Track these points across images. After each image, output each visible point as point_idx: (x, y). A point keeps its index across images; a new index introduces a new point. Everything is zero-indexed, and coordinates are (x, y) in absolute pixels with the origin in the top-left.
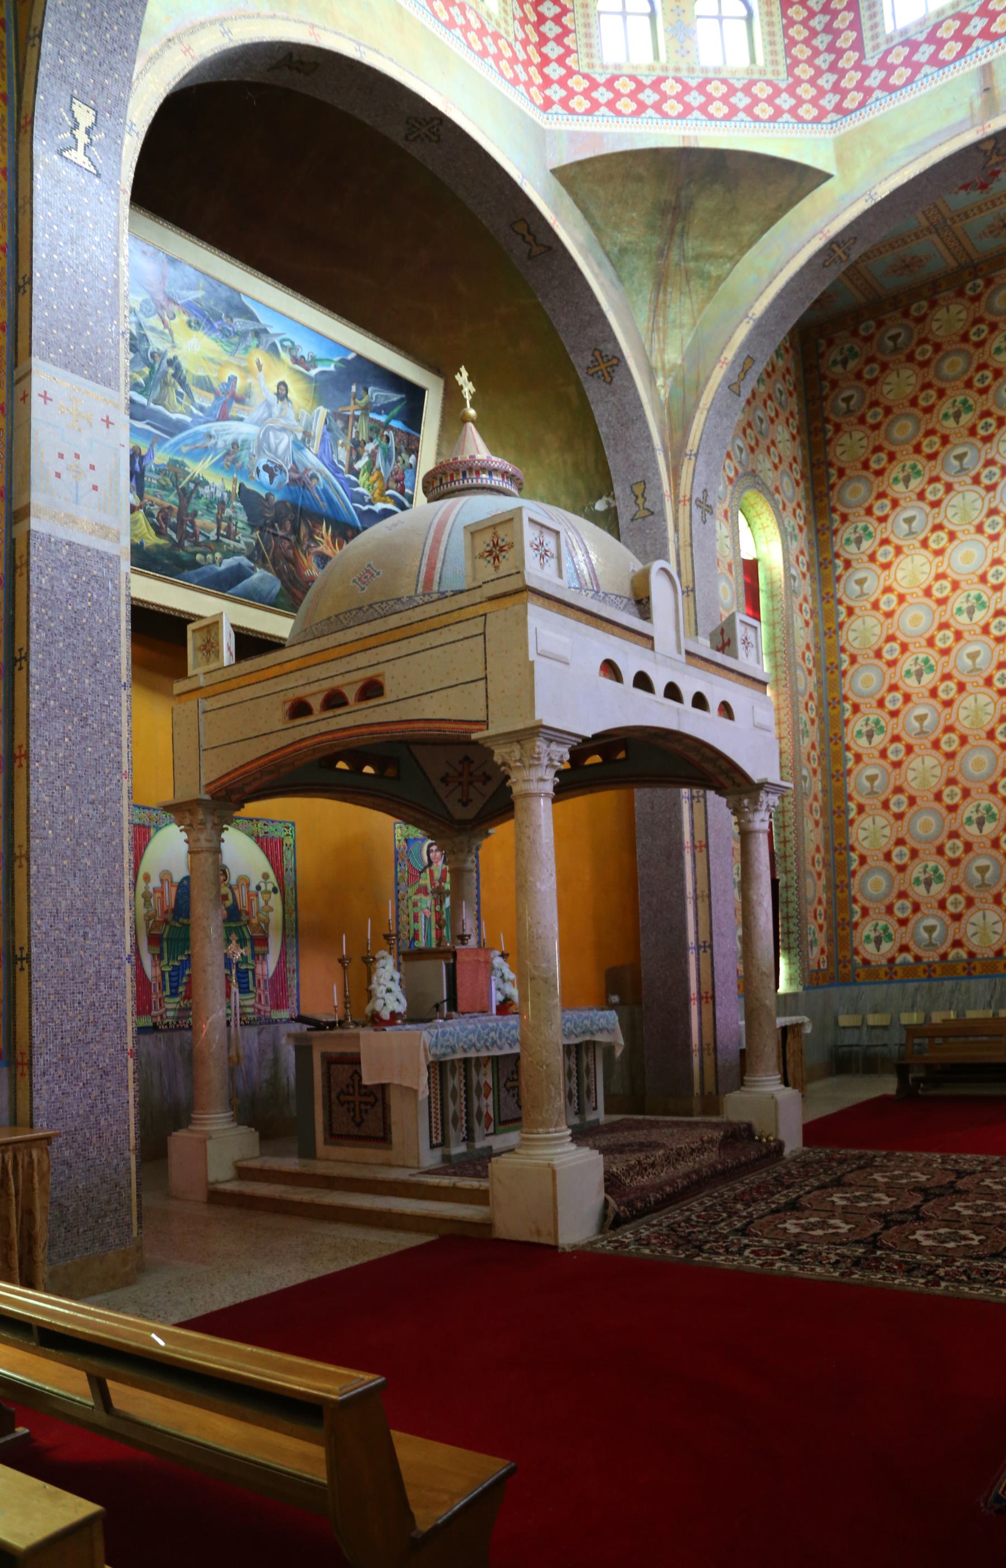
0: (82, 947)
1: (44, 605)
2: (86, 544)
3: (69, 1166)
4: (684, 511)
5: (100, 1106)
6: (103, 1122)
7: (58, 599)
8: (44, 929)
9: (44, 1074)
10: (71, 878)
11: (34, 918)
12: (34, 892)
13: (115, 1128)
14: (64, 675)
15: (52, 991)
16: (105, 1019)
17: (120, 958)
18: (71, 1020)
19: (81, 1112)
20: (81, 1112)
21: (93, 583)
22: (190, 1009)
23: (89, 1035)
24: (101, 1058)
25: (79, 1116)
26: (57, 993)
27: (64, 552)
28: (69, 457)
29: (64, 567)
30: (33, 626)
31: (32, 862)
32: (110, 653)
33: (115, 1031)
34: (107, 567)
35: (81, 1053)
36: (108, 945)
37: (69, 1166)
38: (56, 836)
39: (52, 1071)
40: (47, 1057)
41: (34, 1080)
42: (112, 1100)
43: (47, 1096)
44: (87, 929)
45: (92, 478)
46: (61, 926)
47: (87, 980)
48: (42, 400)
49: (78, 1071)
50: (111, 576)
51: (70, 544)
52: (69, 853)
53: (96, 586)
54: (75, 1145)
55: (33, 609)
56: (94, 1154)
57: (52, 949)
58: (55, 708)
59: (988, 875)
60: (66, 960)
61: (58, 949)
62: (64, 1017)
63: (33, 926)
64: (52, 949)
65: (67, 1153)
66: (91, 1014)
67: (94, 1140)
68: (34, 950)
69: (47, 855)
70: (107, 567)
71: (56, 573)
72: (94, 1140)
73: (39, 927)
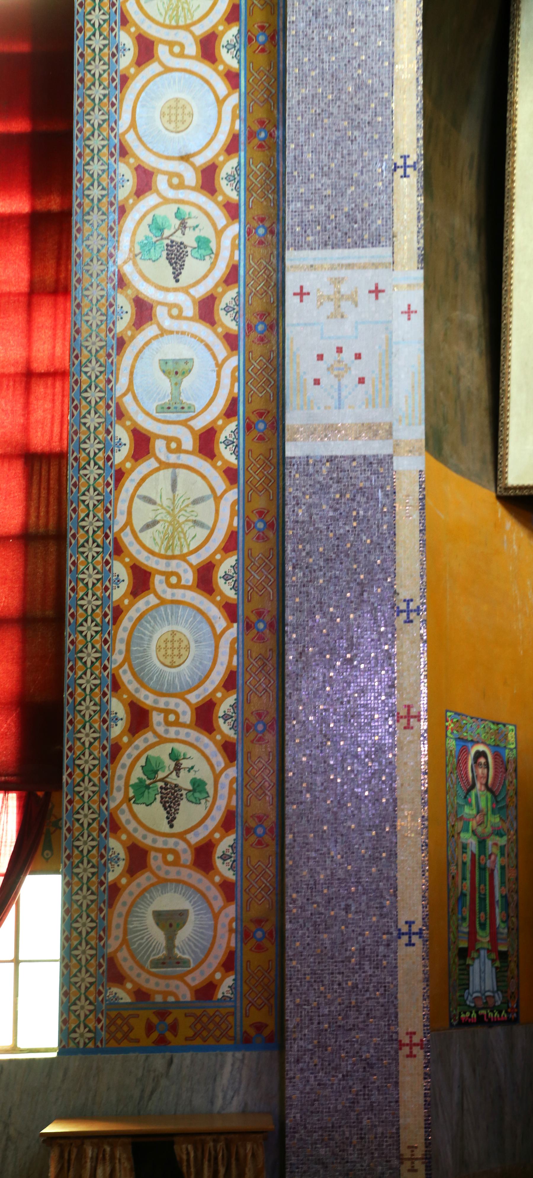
0: (344, 922)
1: (301, 541)
2: (349, 453)
3: (325, 1166)
4: (122, 1172)
5: (362, 1102)
6: (365, 1122)
7: (317, 529)
8: (299, 903)
9: (298, 1061)
10: (330, 844)
11: (289, 891)
12: (289, 863)
13: (380, 1130)
14: (324, 615)
15: (308, 971)
16: (370, 1003)
17: (389, 933)
18: (330, 1003)
19: (340, 1107)
20: (340, 1107)
21: (358, 498)
22: (374, 406)
23: (351, 1021)
24: (364, 1048)
25: (337, 1111)
26: (313, 973)
27: (324, 471)
28: (330, 356)
29: (324, 488)
30: (289, 568)
31: (287, 831)
32: (381, 576)
33: (381, 1018)
34: (376, 473)
35: (341, 1040)
36: (374, 919)
37: (325, 1166)
38: (315, 798)
39: (307, 1058)
40: (301, 1043)
41: (287, 1067)
42: (376, 1097)
43: (301, 1086)
44: (350, 902)
45: (358, 369)
46: (318, 899)
47: (349, 959)
48: (298, 298)
49: (337, 1061)
50: (382, 481)
51: (331, 459)
52: (329, 816)
53: (363, 500)
54: (332, 1143)
55: (289, 548)
56: (354, 1157)
57: (309, 925)
58: (314, 654)
59: (184, 934)
60: (325, 936)
61: (315, 924)
62: (321, 1000)
63: (288, 900)
64: (309, 925)
65: (322, 1151)
66: (353, 997)
67: (355, 1140)
68: (288, 926)
69: (304, 821)
70: (376, 473)
71: (315, 499)
72: (355, 1140)
73: (294, 901)
